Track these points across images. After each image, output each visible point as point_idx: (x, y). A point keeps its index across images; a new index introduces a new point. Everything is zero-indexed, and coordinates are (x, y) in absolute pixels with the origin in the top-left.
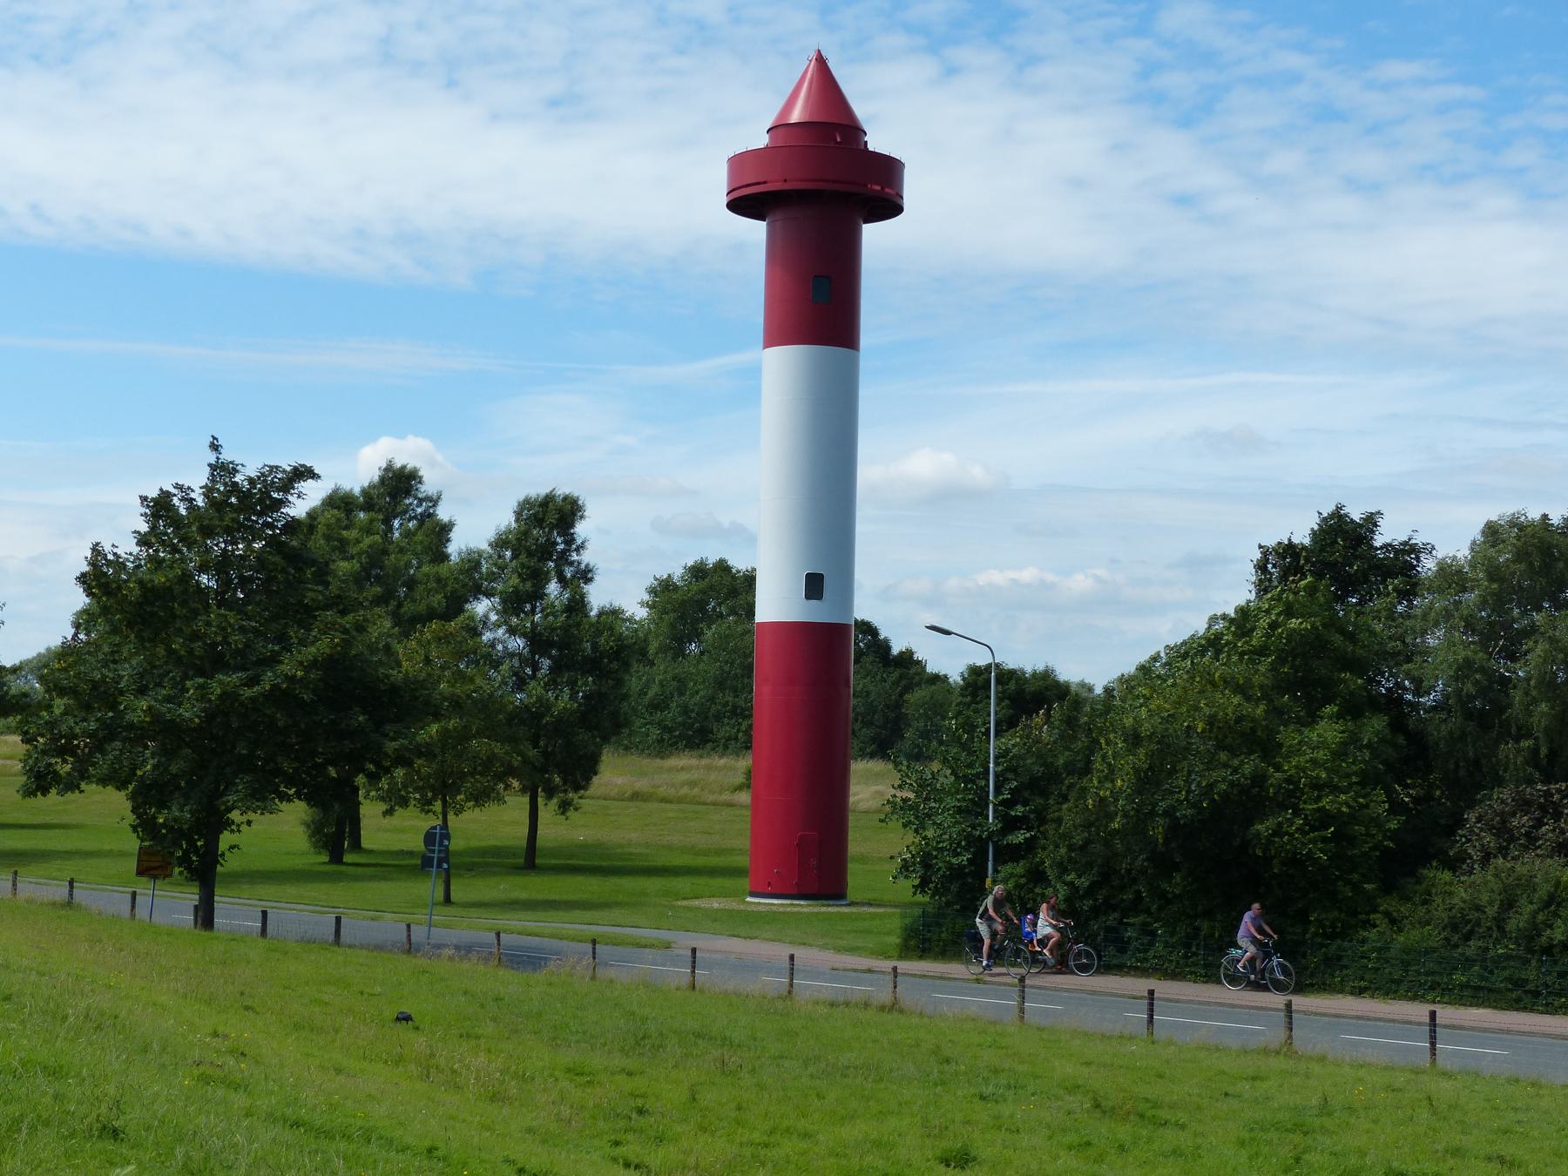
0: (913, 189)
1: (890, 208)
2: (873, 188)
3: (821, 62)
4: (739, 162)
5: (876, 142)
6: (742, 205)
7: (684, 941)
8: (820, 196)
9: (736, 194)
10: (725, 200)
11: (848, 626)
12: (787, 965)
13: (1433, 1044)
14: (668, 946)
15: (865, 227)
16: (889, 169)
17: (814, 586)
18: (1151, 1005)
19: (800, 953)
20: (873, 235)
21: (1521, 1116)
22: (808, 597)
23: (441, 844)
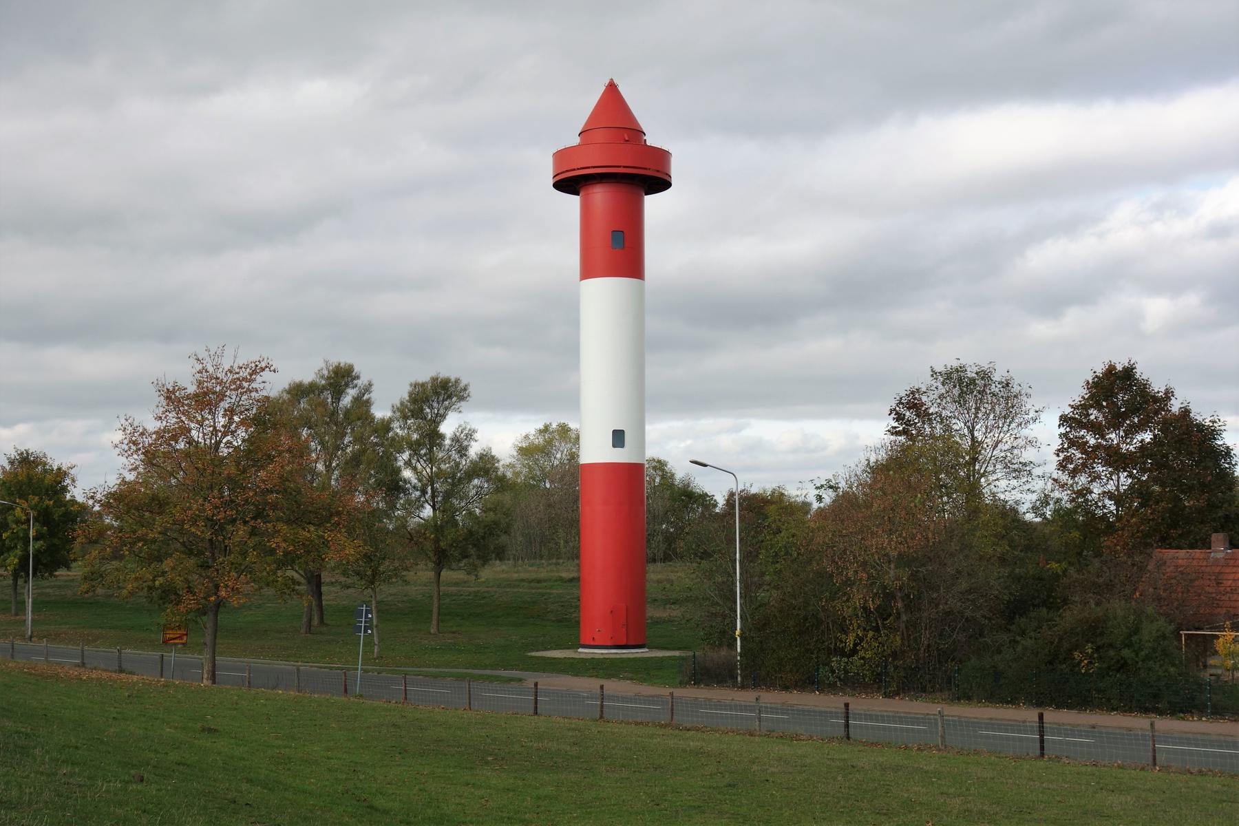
0: (677, 170)
1: (661, 184)
2: (651, 176)
3: (612, 88)
4: (561, 156)
5: (652, 140)
6: (566, 184)
7: (530, 678)
8: (616, 175)
9: (558, 178)
10: (551, 182)
11: (642, 465)
12: (599, 691)
13: (1042, 736)
14: (520, 680)
15: (646, 197)
16: (662, 156)
17: (618, 438)
18: (536, 708)
19: (539, 680)
20: (653, 204)
21: (1026, 487)
22: (614, 446)
23: (366, 617)
